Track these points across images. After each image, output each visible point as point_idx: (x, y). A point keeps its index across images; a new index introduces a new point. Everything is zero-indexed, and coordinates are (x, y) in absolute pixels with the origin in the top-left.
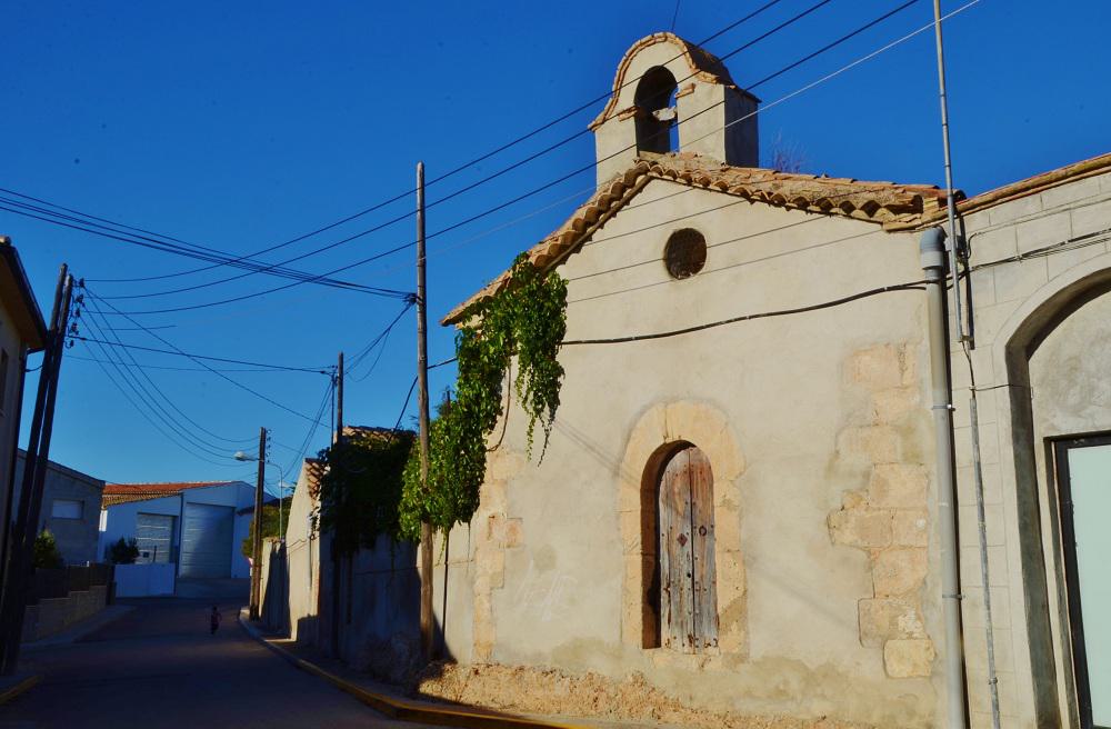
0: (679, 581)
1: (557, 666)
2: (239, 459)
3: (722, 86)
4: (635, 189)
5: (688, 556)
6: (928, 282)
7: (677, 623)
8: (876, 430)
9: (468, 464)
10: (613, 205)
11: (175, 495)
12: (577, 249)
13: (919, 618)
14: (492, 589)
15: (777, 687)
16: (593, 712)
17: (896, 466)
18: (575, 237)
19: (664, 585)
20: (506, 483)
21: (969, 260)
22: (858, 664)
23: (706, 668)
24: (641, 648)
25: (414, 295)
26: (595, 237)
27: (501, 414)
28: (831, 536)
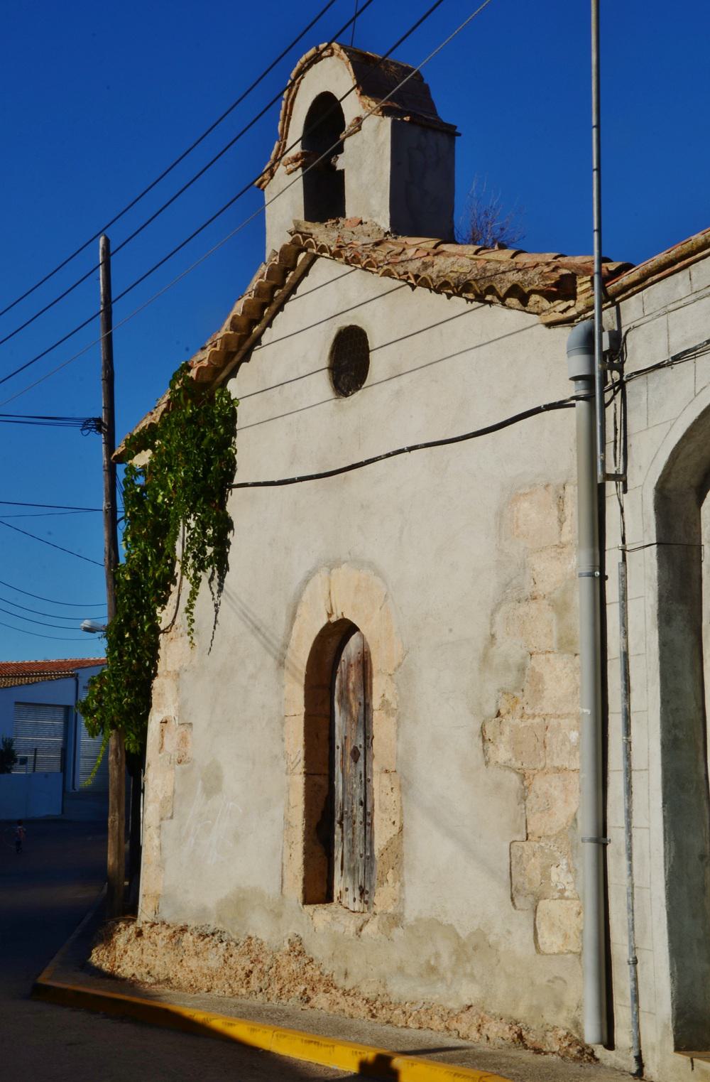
0: (352, 811)
1: (220, 926)
2: (87, 630)
3: (388, 121)
4: (299, 272)
5: (361, 775)
6: (577, 398)
7: (349, 869)
8: (533, 605)
9: (134, 651)
10: (276, 293)
11: (67, 676)
12: (247, 357)
13: (569, 871)
14: (162, 819)
15: (428, 962)
16: (244, 991)
17: (551, 656)
18: (241, 341)
19: (338, 817)
20: (178, 675)
21: (625, 365)
22: (509, 932)
23: (364, 932)
24: (301, 905)
25: (99, 420)
26: (265, 339)
27: (175, 583)
28: (485, 752)
